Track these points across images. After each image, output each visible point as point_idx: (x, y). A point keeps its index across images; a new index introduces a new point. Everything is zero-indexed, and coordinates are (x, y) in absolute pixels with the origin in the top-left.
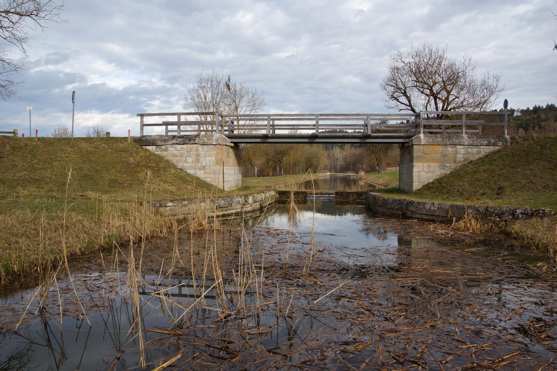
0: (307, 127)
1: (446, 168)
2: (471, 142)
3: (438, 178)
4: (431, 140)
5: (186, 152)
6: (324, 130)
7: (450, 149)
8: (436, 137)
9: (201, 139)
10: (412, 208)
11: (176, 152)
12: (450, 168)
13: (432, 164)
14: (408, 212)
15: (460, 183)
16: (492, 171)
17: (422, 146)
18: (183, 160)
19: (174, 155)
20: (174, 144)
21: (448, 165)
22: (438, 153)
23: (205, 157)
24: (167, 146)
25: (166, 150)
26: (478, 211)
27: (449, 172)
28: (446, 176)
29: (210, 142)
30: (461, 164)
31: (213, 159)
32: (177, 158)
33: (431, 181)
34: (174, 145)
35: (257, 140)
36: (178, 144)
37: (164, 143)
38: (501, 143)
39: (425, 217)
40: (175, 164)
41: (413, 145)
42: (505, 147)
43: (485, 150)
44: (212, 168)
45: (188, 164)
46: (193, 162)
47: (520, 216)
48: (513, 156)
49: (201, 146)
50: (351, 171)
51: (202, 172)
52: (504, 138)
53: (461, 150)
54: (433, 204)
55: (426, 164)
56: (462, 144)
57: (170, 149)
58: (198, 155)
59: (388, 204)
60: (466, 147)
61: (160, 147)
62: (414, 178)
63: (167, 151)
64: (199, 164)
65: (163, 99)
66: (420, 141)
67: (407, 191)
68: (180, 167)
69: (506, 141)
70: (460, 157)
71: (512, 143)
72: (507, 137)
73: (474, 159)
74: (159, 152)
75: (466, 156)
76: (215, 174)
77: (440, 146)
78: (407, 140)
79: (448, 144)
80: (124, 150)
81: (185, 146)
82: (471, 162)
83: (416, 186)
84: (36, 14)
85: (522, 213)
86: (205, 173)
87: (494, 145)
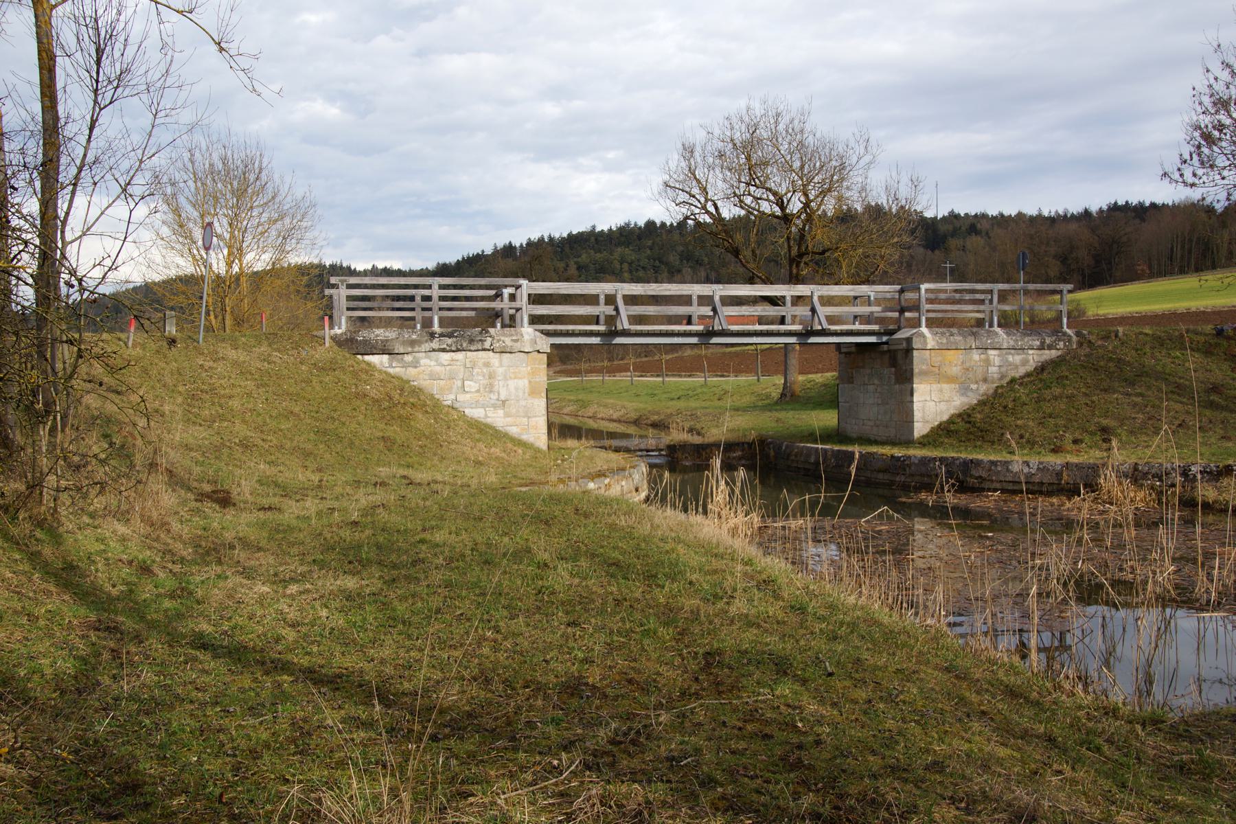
1: (970, 394)
2: (1012, 343)
3: (957, 412)
5: (462, 369)
7: (976, 356)
8: (952, 335)
9: (499, 341)
11: (438, 369)
12: (980, 391)
13: (945, 386)
14: (968, 479)
19: (434, 377)
20: (434, 350)
21: (974, 386)
22: (956, 365)
23: (506, 379)
24: (417, 354)
25: (415, 364)
29: (517, 346)
31: (524, 383)
32: (442, 383)
33: (945, 418)
34: (433, 353)
35: (694, 340)
36: (444, 350)
37: (410, 349)
38: (1061, 344)
40: (436, 396)
44: (523, 403)
46: (478, 391)
48: (1097, 370)
51: (501, 412)
52: (1065, 334)
55: (935, 386)
59: (909, 466)
60: (1004, 352)
62: (916, 413)
63: (416, 367)
64: (492, 396)
66: (925, 343)
67: (854, 435)
68: (449, 403)
71: (1080, 344)
72: (1069, 331)
73: (1017, 376)
74: (398, 370)
75: (1003, 369)
76: (529, 417)
77: (960, 352)
78: (885, 339)
82: (1013, 381)
83: (920, 429)
86: (507, 415)
87: (1050, 347)
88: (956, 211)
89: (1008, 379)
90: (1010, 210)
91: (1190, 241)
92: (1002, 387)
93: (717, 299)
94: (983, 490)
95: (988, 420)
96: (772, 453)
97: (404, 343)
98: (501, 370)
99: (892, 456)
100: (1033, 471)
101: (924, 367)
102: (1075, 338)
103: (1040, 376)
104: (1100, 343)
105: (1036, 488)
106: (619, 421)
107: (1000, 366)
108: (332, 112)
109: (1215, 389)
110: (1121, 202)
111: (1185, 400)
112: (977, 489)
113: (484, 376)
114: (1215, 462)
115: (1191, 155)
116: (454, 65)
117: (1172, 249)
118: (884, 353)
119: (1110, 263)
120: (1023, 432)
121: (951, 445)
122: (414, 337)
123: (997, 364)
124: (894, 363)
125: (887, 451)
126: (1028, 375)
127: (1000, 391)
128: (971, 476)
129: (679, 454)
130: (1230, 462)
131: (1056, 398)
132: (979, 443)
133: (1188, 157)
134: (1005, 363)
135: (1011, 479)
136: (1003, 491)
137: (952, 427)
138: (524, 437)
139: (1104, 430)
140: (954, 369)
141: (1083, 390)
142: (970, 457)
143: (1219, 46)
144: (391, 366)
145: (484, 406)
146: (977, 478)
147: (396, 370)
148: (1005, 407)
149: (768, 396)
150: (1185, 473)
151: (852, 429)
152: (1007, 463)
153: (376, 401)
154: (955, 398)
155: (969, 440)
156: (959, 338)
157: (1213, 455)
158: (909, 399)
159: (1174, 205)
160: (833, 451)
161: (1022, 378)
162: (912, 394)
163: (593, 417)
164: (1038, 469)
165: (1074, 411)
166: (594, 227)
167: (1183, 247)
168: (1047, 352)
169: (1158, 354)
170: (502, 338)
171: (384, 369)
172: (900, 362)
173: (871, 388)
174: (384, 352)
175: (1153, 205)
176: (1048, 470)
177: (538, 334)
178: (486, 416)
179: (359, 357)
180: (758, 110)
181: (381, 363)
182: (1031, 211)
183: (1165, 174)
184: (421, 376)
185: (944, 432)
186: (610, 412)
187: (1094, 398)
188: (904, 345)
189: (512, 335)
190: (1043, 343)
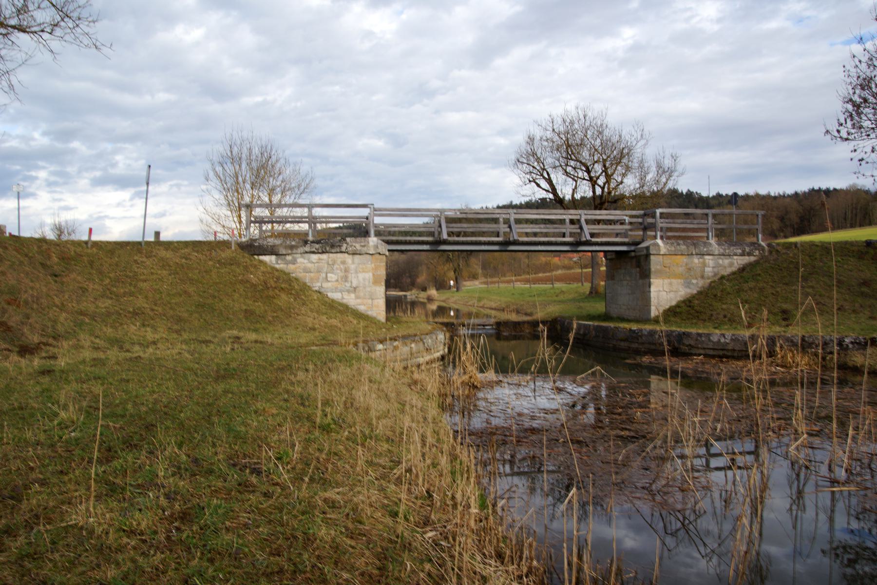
0: (298, 220)
1: (692, 286)
2: (722, 251)
3: (682, 299)
4: (673, 249)
5: (326, 265)
6: (341, 225)
7: (696, 260)
8: (679, 244)
9: (351, 246)
10: (686, 342)
11: (309, 265)
12: (697, 285)
13: (674, 281)
14: (681, 346)
15: (724, 306)
16: (762, 290)
17: (661, 257)
18: (321, 278)
19: (306, 270)
20: (306, 252)
21: (694, 281)
22: (681, 266)
23: (356, 272)
24: (295, 255)
25: (294, 262)
26: (792, 341)
27: (695, 292)
28: (693, 297)
29: (365, 250)
30: (709, 281)
31: (369, 276)
32: (312, 275)
33: (674, 303)
34: (306, 255)
35: (496, 248)
36: (313, 252)
37: (290, 252)
38: (757, 253)
39: (711, 352)
40: (308, 284)
41: (650, 254)
42: (762, 257)
43: (739, 261)
44: (368, 289)
45: (329, 285)
46: (337, 281)
47: (851, 346)
48: (781, 270)
49: (351, 256)
50: (393, 287)
51: (353, 296)
52: (760, 245)
53: (710, 261)
54: (724, 335)
55: (667, 281)
56: (711, 253)
57: (300, 260)
58: (346, 271)
59: (641, 336)
60: (716, 257)
61: (283, 257)
62: (652, 300)
63: (294, 264)
64: (347, 284)
65: (52, 168)
66: (660, 250)
67: (615, 316)
68: (317, 289)
69: (763, 249)
70: (709, 271)
71: (770, 252)
72: (763, 244)
73: (726, 274)
74: (282, 266)
75: (716, 270)
76: (372, 299)
77: (684, 257)
78: (633, 248)
79: (694, 253)
80: (232, 262)
81: (324, 256)
82: (723, 277)
83: (654, 313)
84: (49, 31)
85: (852, 343)
86: (357, 297)
87: (749, 254)
88: (721, 193)
89: (719, 276)
90: (751, 192)
91: (856, 209)
92: (714, 282)
93: (512, 219)
94: (692, 354)
95: (703, 304)
96: (559, 327)
97: (286, 247)
98: (353, 267)
99: (630, 330)
100: (727, 341)
101: (658, 267)
102: (766, 247)
103: (741, 274)
104: (784, 251)
105: (729, 354)
106: (495, 309)
107: (713, 267)
108: (379, 144)
109: (865, 283)
110: (816, 188)
111: (843, 291)
112: (686, 355)
113: (341, 271)
114: (863, 335)
115: (846, 120)
116: (454, 118)
117: (846, 214)
118: (632, 258)
119: (809, 221)
120: (726, 313)
121: (676, 322)
122: (293, 243)
123: (711, 265)
124: (638, 265)
125: (627, 326)
126: (734, 273)
127: (713, 284)
128: (684, 344)
129: (502, 328)
130: (875, 335)
131: (751, 289)
132: (695, 321)
133: (843, 122)
134: (717, 265)
135: (711, 347)
136: (705, 356)
137: (678, 310)
138: (370, 313)
139: (784, 312)
140: (680, 268)
141: (771, 284)
142: (683, 330)
143: (861, 39)
144: (277, 263)
145: (341, 291)
146: (687, 346)
147: (281, 266)
148: (715, 296)
149: (584, 293)
150: (840, 343)
151: (614, 312)
152: (709, 335)
153: (254, 286)
154: (681, 289)
155: (688, 319)
156: (683, 247)
157: (862, 330)
158: (647, 289)
159: (847, 189)
160: (594, 326)
161: (729, 275)
162: (650, 287)
163: (482, 307)
164: (732, 339)
165: (763, 298)
166: (511, 202)
167: (852, 212)
168: (747, 258)
169: (825, 259)
170: (354, 244)
171: (272, 265)
172: (643, 264)
173: (625, 283)
174: (272, 254)
175: (835, 190)
176: (739, 340)
177: (380, 242)
178: (343, 298)
179: (256, 257)
180: (574, 112)
181: (271, 261)
182: (763, 192)
183: (827, 132)
184: (298, 270)
185: (672, 313)
186: (494, 305)
187: (778, 289)
188: (645, 251)
189: (361, 242)
190: (744, 251)
